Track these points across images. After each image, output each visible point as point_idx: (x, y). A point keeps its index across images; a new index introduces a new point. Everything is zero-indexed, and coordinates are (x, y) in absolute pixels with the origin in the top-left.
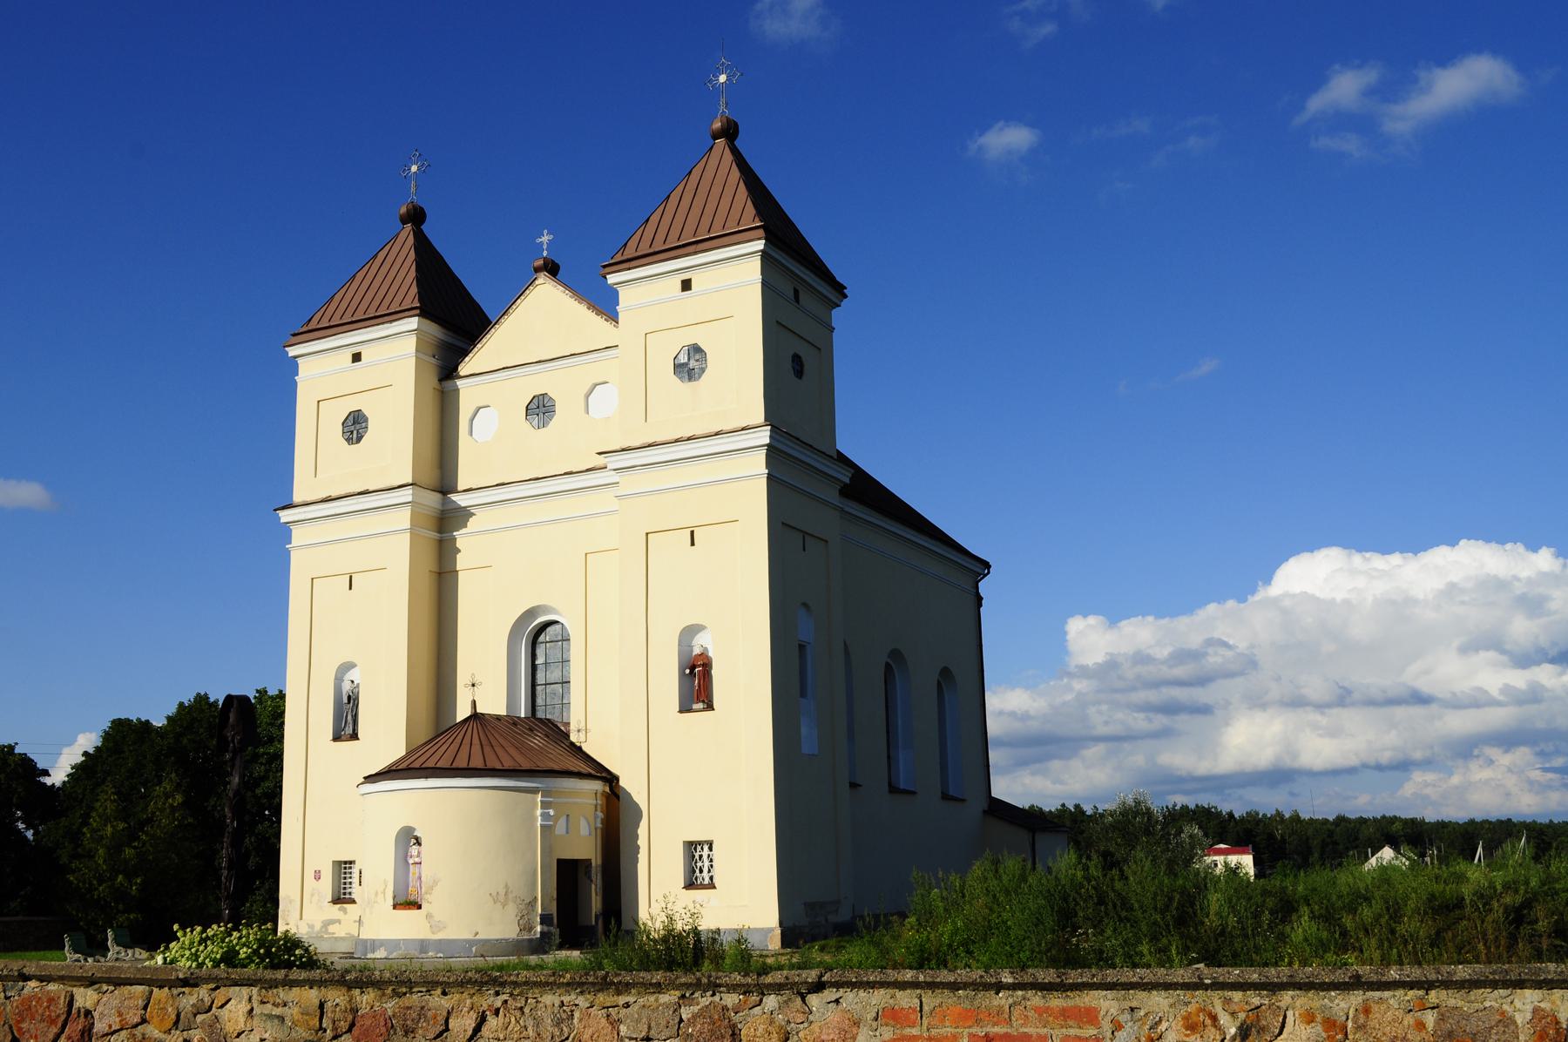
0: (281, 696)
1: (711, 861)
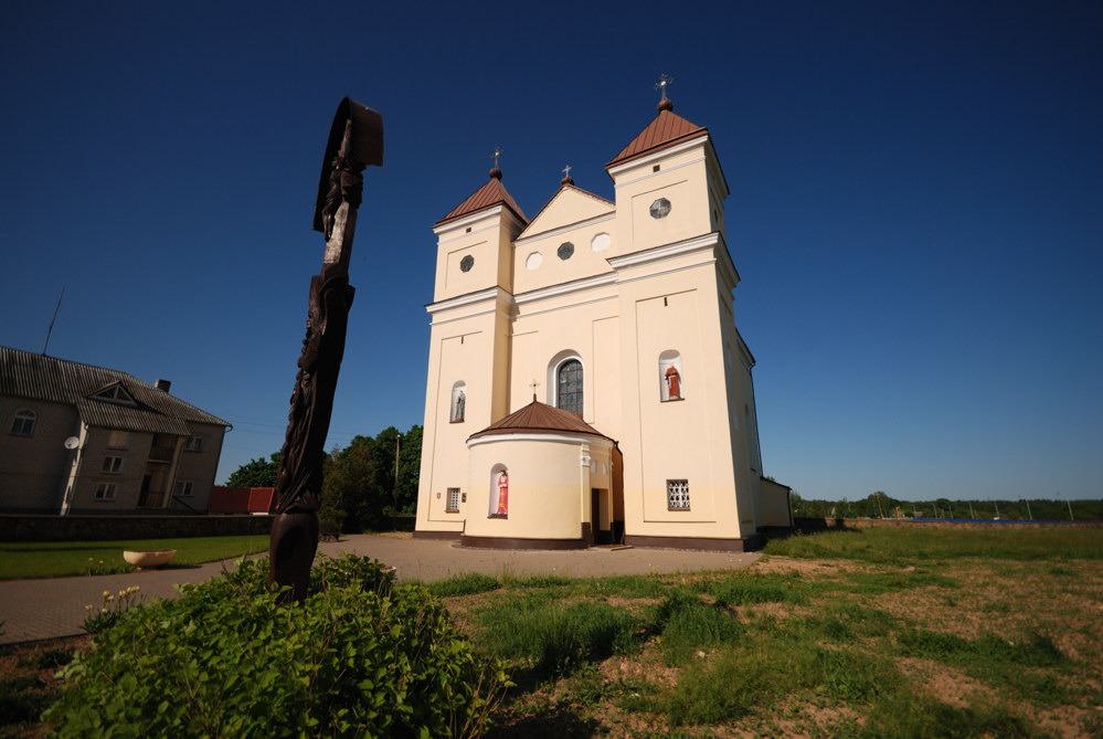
0: (422, 428)
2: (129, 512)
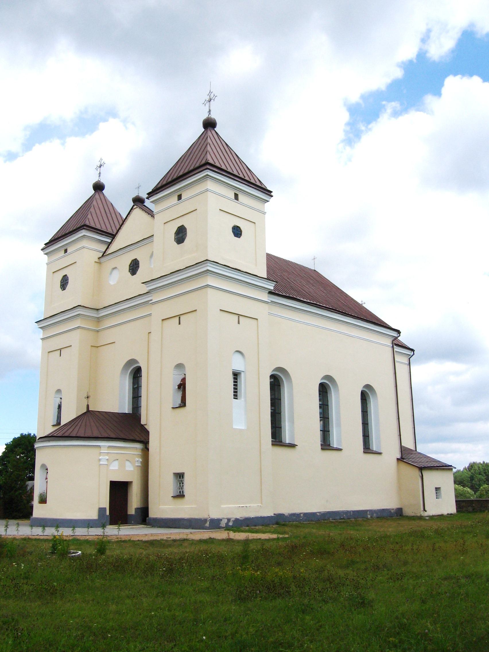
1: (183, 484)
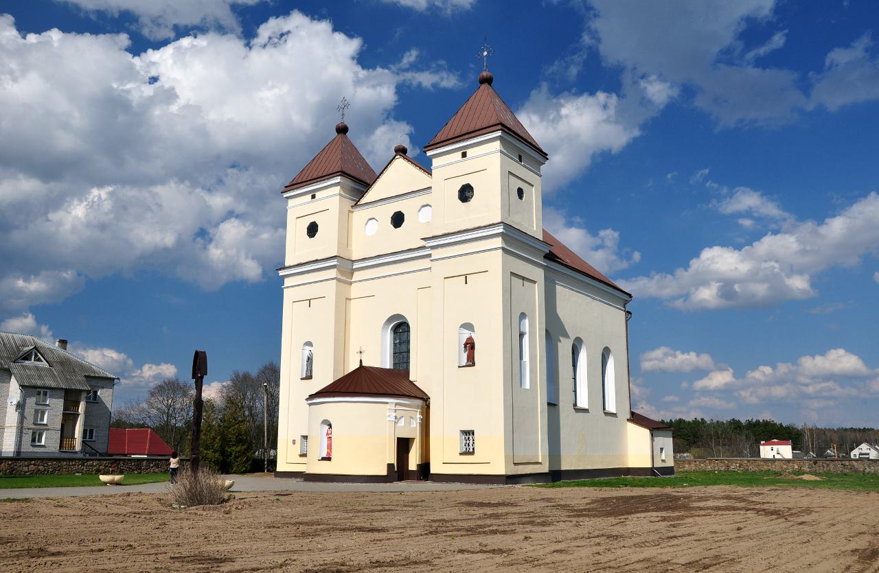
2: (562, 285)
